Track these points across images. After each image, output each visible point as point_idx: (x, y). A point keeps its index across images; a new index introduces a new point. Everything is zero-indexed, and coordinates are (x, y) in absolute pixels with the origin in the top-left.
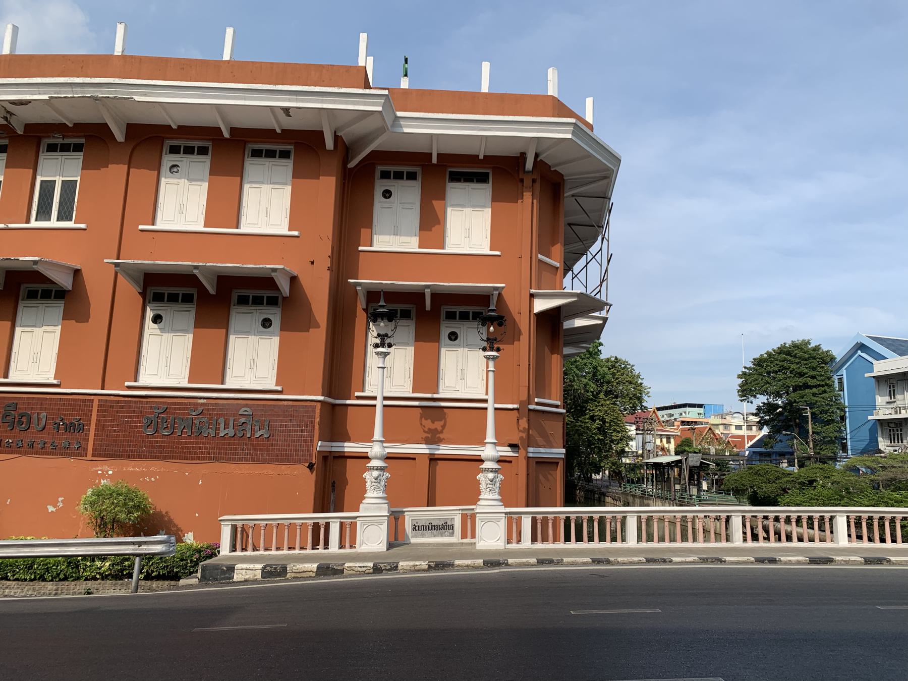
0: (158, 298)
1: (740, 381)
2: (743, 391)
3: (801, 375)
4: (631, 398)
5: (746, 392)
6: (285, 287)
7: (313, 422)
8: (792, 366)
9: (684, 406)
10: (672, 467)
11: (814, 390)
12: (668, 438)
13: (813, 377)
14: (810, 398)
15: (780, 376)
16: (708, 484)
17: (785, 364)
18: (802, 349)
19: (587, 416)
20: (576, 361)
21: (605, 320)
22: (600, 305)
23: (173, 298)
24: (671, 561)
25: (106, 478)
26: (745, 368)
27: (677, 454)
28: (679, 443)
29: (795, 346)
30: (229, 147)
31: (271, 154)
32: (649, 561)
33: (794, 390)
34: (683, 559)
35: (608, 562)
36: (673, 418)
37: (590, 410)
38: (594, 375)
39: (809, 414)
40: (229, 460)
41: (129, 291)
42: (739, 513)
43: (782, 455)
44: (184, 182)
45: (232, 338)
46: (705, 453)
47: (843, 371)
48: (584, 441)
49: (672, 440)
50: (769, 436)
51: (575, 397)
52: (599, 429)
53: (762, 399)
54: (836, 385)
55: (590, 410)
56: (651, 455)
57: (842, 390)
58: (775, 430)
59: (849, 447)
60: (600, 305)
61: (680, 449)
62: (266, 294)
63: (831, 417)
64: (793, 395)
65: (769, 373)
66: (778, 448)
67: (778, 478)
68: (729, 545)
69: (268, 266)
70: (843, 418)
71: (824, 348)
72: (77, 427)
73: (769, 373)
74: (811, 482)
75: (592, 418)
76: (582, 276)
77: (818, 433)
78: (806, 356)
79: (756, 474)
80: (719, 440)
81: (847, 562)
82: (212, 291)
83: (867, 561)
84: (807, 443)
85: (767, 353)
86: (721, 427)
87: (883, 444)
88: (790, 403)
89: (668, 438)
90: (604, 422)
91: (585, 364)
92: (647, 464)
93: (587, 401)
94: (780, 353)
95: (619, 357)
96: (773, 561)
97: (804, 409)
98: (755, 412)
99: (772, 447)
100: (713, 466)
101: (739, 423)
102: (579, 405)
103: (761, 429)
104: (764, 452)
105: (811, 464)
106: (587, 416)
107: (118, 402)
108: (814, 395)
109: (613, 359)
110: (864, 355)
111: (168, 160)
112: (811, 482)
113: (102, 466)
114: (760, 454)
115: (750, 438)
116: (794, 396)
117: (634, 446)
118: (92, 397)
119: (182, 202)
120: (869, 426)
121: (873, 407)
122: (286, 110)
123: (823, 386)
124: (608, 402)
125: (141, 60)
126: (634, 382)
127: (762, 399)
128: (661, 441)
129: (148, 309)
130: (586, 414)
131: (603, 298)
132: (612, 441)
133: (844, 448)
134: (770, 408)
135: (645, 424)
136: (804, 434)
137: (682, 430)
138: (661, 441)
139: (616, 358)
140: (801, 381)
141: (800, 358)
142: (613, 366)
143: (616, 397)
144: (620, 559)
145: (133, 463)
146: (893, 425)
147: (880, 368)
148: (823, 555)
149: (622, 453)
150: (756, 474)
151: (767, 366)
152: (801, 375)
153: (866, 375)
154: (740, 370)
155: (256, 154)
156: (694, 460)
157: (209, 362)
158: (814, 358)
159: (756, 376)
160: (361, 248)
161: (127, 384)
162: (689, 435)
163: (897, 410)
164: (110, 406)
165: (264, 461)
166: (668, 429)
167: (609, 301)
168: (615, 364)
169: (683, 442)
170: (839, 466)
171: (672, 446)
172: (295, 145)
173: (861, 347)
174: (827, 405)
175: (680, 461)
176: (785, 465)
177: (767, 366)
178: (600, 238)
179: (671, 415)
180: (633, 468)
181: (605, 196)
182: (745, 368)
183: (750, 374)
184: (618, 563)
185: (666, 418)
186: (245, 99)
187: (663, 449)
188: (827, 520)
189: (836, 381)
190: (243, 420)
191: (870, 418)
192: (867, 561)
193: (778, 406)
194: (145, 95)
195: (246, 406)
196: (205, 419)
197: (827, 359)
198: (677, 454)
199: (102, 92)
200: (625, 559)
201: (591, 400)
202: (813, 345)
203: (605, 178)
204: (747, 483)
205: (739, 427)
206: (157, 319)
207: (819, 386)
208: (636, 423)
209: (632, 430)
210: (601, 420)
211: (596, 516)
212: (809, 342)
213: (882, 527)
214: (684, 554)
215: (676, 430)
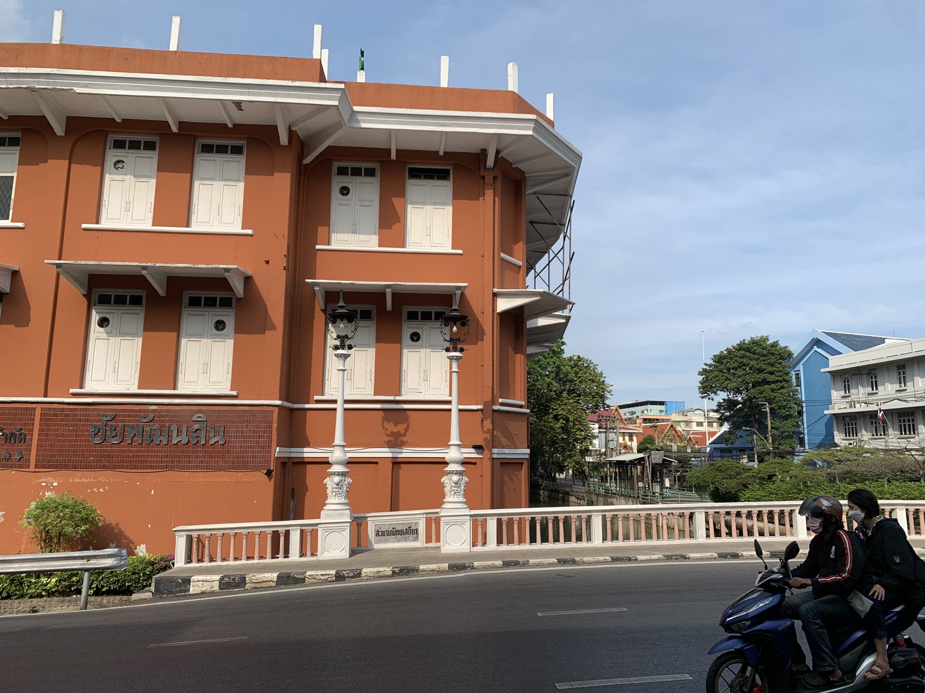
0: (104, 300)
1: (701, 378)
2: (704, 388)
3: (760, 371)
5: (707, 388)
6: (238, 287)
7: (270, 427)
11: (773, 386)
12: (631, 436)
13: (771, 373)
15: (740, 372)
16: (670, 481)
17: (745, 360)
18: (760, 345)
19: (551, 416)
23: (120, 301)
25: (51, 490)
26: (706, 364)
27: (639, 451)
28: (641, 440)
29: (754, 342)
30: (177, 143)
31: (222, 150)
33: (754, 387)
34: (648, 557)
35: (574, 562)
36: (635, 416)
37: (554, 410)
38: (557, 375)
39: (768, 409)
40: (182, 468)
41: (72, 293)
43: (742, 450)
44: (129, 179)
45: (184, 341)
47: (800, 367)
49: (635, 438)
50: (730, 432)
52: (562, 428)
53: (722, 396)
54: (794, 380)
55: (554, 410)
56: (614, 453)
57: (799, 385)
58: (736, 426)
59: (806, 441)
61: (643, 446)
62: (218, 295)
63: (789, 412)
65: (729, 369)
66: (738, 443)
67: (739, 474)
68: (692, 541)
69: (221, 266)
70: (800, 413)
71: (782, 344)
72: (18, 438)
73: (729, 369)
74: (770, 477)
75: (556, 418)
76: (544, 275)
77: (776, 429)
78: (765, 352)
80: (681, 437)
82: (162, 292)
85: (727, 349)
86: (683, 424)
87: (839, 438)
88: (750, 399)
90: (567, 420)
93: (550, 400)
94: (739, 350)
95: (581, 356)
96: (735, 556)
97: (762, 405)
98: (715, 408)
99: (732, 443)
101: (700, 419)
103: (721, 425)
104: (725, 448)
105: (770, 459)
106: (551, 416)
107: (63, 410)
108: (773, 390)
110: (819, 350)
111: (112, 155)
112: (770, 477)
113: (46, 477)
114: (722, 450)
115: (712, 434)
118: (34, 406)
119: (128, 200)
120: (825, 420)
121: (829, 402)
122: (238, 104)
125: (81, 49)
127: (722, 396)
129: (94, 312)
134: (730, 404)
135: (608, 422)
136: (763, 429)
137: (644, 428)
139: (579, 357)
140: (760, 377)
141: (759, 354)
142: (576, 365)
143: (579, 395)
144: (585, 559)
145: (79, 474)
146: (847, 419)
147: (836, 363)
149: (585, 452)
151: (727, 362)
152: (760, 371)
153: (822, 370)
155: (207, 149)
157: (160, 366)
158: (773, 354)
159: (716, 373)
160: (318, 247)
161: (72, 391)
162: (651, 432)
164: (55, 415)
165: (219, 469)
166: (631, 426)
168: (578, 363)
169: (645, 439)
170: (797, 460)
171: (635, 444)
172: (248, 140)
173: (817, 342)
174: (785, 400)
175: (642, 459)
177: (727, 362)
178: (562, 236)
179: (633, 413)
180: (596, 467)
181: (566, 194)
182: (706, 364)
183: (710, 371)
184: (584, 563)
185: (628, 416)
186: (194, 92)
189: (794, 377)
190: (197, 426)
191: (826, 412)
193: (737, 403)
194: (86, 86)
195: (200, 411)
196: (157, 426)
199: (39, 83)
200: (591, 559)
201: (555, 399)
202: (771, 341)
203: (567, 175)
205: (700, 424)
206: (103, 322)
207: (778, 381)
214: (649, 551)
215: (638, 428)
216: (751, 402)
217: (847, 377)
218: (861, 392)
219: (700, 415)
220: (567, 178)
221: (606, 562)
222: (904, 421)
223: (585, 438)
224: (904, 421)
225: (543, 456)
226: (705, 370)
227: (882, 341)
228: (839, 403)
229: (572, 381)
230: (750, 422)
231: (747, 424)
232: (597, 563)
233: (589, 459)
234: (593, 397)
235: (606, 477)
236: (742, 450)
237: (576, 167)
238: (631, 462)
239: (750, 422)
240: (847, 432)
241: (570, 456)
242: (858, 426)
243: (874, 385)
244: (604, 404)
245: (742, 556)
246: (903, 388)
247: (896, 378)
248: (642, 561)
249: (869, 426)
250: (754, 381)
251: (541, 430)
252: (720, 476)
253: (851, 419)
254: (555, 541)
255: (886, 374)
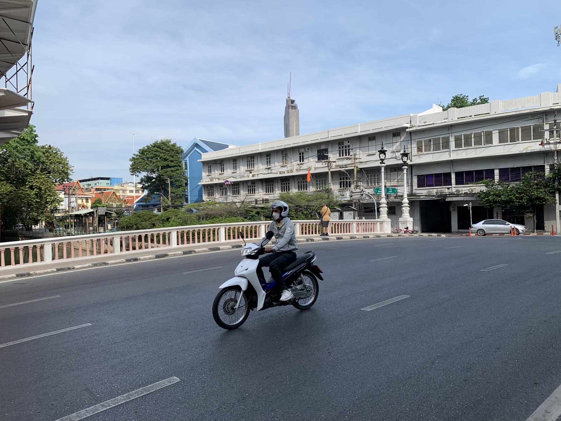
1: (131, 163)
2: (133, 169)
3: (166, 160)
4: (60, 174)
5: (134, 169)
8: (161, 155)
9: (98, 179)
10: (87, 216)
11: (172, 169)
12: (87, 199)
13: (172, 161)
14: (170, 173)
15: (154, 160)
16: (111, 226)
17: (157, 153)
18: (166, 145)
19: (27, 186)
20: (17, 147)
21: (30, 113)
22: (24, 102)
24: (74, 268)
26: (134, 155)
27: (92, 208)
28: (93, 202)
29: (163, 143)
32: (58, 270)
33: (162, 169)
34: (82, 266)
35: (29, 275)
36: (90, 187)
37: (29, 182)
38: (32, 157)
39: (169, 182)
42: (118, 236)
43: (155, 206)
46: (109, 207)
47: (187, 159)
48: (25, 203)
49: (90, 201)
50: (148, 196)
51: (17, 172)
52: (36, 194)
53: (143, 174)
54: (184, 166)
55: (29, 182)
56: (74, 210)
57: (186, 169)
58: (151, 192)
59: (189, 200)
60: (24, 102)
61: (94, 205)
63: (180, 184)
64: (161, 171)
65: (148, 158)
66: (153, 202)
67: (150, 218)
68: (112, 254)
70: (186, 184)
71: (178, 145)
73: (148, 158)
74: (168, 219)
75: (31, 188)
76: (13, 80)
77: (173, 193)
78: (169, 149)
79: (138, 217)
80: (119, 200)
81: (174, 255)
83: (185, 253)
84: (168, 198)
85: (147, 146)
86: (121, 192)
87: (205, 197)
88: (159, 176)
89: (87, 199)
90: (40, 189)
91: (24, 149)
92: (71, 216)
93: (27, 176)
94: (154, 147)
95: (52, 146)
96: (136, 260)
97: (166, 179)
98: (139, 181)
99: (149, 202)
100: (114, 215)
101: (131, 189)
102: (21, 179)
103: (143, 191)
104: (145, 204)
105: (171, 209)
106: (27, 186)
108: (172, 171)
109: (47, 147)
110: (198, 150)
112: (168, 219)
114: (143, 206)
115: (137, 197)
116: (161, 172)
117: (63, 206)
120: (199, 188)
121: (201, 178)
123: (177, 166)
124: (43, 176)
126: (63, 163)
127: (143, 174)
128: (82, 201)
130: (26, 185)
131: (29, 98)
132: (47, 203)
133: (187, 200)
134: (149, 179)
135: (69, 191)
136: (166, 193)
137: (96, 194)
138: (82, 201)
139: (50, 146)
140: (165, 163)
141: (165, 150)
142: (47, 152)
143: (49, 173)
144: (37, 272)
146: (209, 187)
147: (206, 157)
148: (163, 253)
149: (56, 210)
150: (138, 217)
151: (147, 154)
152: (166, 160)
153: (198, 161)
154: (131, 156)
156: (102, 211)
158: (173, 150)
159: (140, 160)
162: (100, 196)
163: (212, 179)
166: (87, 193)
167: (33, 100)
168: (48, 150)
169: (96, 201)
170: (183, 210)
171: (89, 204)
173: (196, 145)
174: (179, 177)
175: (93, 213)
176: (156, 212)
177: (147, 154)
178: (26, 54)
179: (89, 185)
180: (62, 219)
181: (27, 21)
182: (134, 155)
183: (137, 159)
185: (86, 187)
187: (83, 207)
188: (167, 234)
189: (184, 164)
191: (199, 184)
192: (185, 253)
193: (153, 178)
197: (179, 151)
198: (92, 208)
200: (42, 271)
201: (30, 174)
202: (172, 143)
203: (26, 7)
204: (133, 222)
205: (131, 191)
207: (175, 166)
208: (64, 190)
209: (62, 195)
210: (38, 189)
211: (21, 247)
212: (170, 141)
213: (193, 235)
214: (82, 262)
215: (92, 194)
216: (160, 178)
217: (210, 164)
218: (216, 173)
219: (131, 186)
220: (27, 9)
221: (53, 272)
222: (301, 182)
223: (53, 201)
224: (301, 182)
225: (21, 214)
226: (134, 158)
227: (227, 146)
228: (206, 180)
229: (43, 163)
230: (160, 189)
231: (158, 190)
232: (46, 273)
233: (56, 215)
234: (60, 174)
235: (68, 226)
236: (155, 206)
237: (34, 2)
238: (86, 215)
239: (160, 189)
240: (209, 194)
241: (42, 213)
242: (290, 185)
243: (223, 170)
244: (68, 178)
245: (140, 259)
246: (302, 162)
247: (281, 159)
248: (77, 269)
249: (219, 191)
250: (162, 167)
251: (19, 196)
252: (139, 220)
253: (252, 183)
254: (16, 264)
255: (241, 160)
